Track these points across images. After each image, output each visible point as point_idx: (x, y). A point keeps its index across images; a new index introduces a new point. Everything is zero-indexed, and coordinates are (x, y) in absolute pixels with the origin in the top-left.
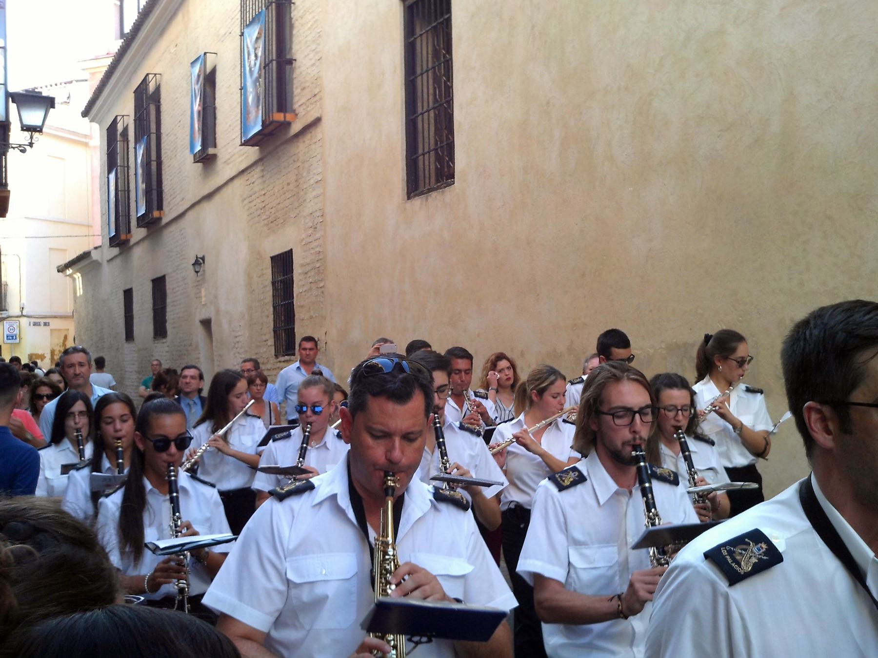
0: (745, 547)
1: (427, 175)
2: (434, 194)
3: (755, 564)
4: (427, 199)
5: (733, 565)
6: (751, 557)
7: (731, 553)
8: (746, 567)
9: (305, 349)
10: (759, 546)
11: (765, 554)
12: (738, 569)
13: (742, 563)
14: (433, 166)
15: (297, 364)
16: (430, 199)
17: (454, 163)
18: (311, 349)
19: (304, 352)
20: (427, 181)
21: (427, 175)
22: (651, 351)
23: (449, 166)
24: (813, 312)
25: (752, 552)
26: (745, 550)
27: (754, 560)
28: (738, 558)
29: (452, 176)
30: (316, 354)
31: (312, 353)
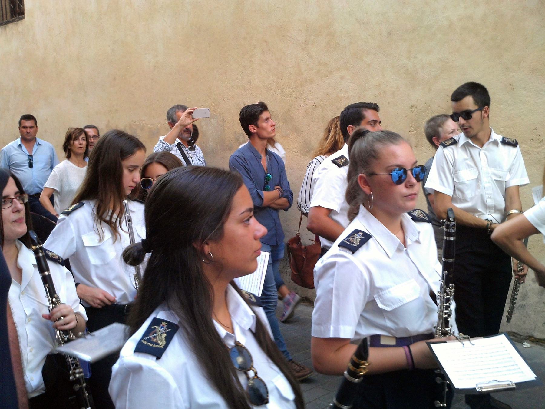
0: (155, 331)
1: (4, 12)
2: (10, 25)
3: (165, 337)
4: (5, 28)
5: (154, 346)
6: (161, 335)
7: (149, 340)
8: (162, 343)
9: (25, 127)
10: (161, 325)
11: (167, 328)
12: (159, 346)
13: (159, 342)
14: (8, 7)
15: (19, 141)
16: (7, 29)
17: (23, 5)
18: (31, 127)
19: (24, 130)
20: (5, 16)
21: (4, 12)
22: (159, 126)
23: (20, 7)
24: (134, 137)
25: (160, 331)
26: (155, 333)
27: (164, 335)
28: (154, 341)
29: (22, 13)
30: (36, 131)
31: (32, 130)
